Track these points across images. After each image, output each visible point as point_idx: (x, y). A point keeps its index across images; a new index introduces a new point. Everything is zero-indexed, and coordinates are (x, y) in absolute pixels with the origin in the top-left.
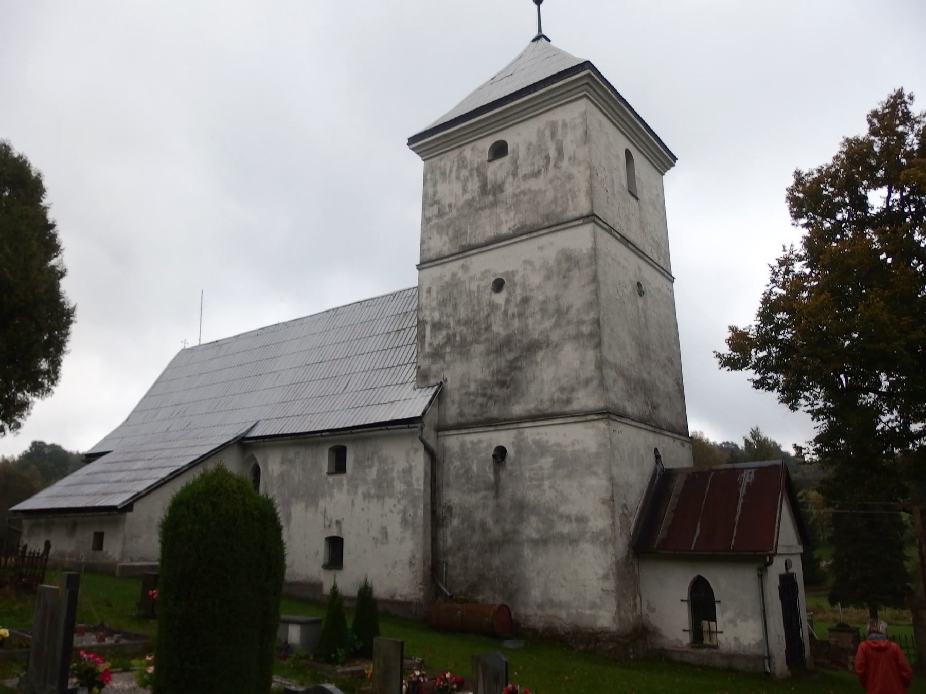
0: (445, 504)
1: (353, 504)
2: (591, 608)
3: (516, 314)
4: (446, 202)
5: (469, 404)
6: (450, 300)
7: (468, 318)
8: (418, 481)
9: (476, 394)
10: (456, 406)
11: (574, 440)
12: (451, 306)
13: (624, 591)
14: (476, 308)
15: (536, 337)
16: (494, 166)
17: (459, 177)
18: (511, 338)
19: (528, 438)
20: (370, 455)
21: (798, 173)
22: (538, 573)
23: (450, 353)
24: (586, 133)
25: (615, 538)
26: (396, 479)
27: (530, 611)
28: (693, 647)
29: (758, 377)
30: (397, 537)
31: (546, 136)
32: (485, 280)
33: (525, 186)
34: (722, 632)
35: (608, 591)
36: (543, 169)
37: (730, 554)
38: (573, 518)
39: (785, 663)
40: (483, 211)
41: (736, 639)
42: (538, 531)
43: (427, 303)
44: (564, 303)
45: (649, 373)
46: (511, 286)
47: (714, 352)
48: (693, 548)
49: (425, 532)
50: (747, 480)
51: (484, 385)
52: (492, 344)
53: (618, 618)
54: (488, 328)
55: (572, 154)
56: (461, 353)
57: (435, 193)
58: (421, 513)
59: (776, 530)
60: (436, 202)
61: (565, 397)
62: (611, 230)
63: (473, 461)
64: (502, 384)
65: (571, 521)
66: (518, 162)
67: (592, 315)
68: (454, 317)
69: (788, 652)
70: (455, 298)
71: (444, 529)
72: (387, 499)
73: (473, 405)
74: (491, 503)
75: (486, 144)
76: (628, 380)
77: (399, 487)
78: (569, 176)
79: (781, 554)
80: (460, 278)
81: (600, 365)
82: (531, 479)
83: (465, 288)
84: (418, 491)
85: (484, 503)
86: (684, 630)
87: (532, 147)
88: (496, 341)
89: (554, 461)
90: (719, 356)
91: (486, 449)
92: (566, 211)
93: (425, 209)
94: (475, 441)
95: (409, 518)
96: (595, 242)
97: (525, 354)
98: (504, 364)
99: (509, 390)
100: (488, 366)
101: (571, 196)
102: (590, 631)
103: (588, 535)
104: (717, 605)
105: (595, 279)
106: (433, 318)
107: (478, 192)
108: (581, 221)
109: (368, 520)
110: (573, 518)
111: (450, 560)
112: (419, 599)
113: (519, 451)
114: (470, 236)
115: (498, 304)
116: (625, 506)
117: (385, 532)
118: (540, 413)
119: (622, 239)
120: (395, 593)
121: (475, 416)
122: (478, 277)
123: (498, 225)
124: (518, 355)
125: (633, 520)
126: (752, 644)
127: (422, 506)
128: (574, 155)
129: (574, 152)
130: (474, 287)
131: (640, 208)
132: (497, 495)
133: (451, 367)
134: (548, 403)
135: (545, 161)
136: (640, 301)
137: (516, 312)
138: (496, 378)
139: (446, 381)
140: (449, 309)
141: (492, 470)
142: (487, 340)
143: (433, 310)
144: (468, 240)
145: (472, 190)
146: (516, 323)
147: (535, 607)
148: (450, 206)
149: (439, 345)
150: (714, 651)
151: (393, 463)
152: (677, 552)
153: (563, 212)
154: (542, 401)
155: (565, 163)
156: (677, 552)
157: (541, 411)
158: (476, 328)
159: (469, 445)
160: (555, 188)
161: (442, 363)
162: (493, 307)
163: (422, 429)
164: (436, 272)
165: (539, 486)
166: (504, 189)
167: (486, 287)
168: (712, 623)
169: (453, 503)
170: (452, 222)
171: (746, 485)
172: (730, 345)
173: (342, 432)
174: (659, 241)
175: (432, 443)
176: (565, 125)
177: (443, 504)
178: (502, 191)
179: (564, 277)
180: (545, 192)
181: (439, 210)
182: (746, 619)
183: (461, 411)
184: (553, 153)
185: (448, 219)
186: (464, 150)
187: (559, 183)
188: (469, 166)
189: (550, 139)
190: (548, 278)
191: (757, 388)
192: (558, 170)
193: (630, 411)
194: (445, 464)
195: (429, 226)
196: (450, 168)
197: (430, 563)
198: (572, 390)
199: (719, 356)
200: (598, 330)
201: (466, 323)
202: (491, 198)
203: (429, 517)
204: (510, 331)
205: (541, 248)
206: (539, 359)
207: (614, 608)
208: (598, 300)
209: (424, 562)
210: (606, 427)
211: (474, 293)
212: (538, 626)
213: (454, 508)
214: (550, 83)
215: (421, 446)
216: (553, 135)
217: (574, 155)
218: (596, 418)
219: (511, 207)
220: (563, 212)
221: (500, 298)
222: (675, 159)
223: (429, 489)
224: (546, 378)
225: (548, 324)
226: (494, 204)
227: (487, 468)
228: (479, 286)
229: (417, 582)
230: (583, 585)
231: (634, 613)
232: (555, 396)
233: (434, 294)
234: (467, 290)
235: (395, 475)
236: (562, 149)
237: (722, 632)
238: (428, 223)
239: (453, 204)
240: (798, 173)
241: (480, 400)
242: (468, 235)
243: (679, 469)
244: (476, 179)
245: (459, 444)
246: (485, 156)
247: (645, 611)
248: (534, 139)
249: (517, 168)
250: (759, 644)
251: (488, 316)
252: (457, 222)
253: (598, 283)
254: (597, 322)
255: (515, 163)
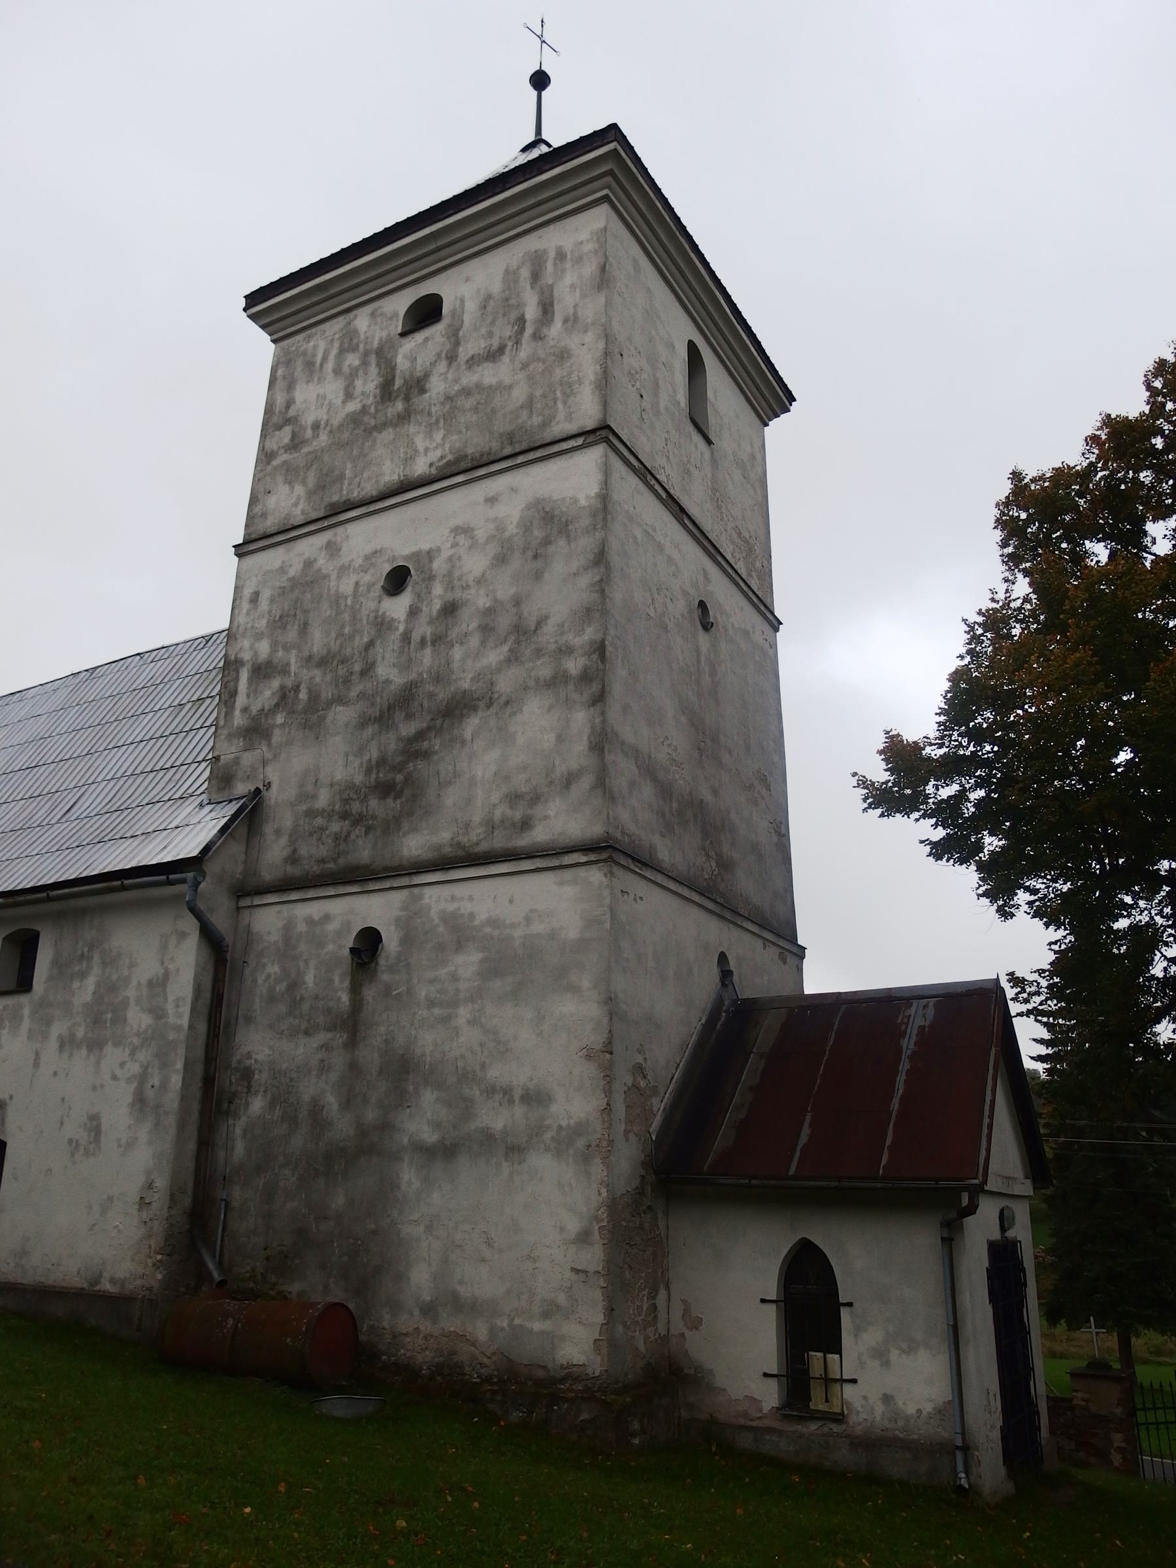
0: (239, 1062)
1: (36, 1064)
2: (546, 1315)
3: (428, 638)
4: (309, 419)
5: (311, 834)
6: (295, 615)
7: (329, 651)
8: (177, 1006)
9: (328, 814)
10: (284, 840)
11: (532, 911)
12: (296, 627)
13: (628, 1275)
14: (346, 630)
15: (465, 685)
16: (413, 344)
17: (340, 370)
18: (414, 691)
19: (430, 909)
20: (86, 950)
21: (1016, 476)
22: (429, 1228)
23: (283, 725)
24: (603, 269)
25: (611, 1142)
26: (132, 1002)
27: (405, 1322)
28: (786, 1417)
29: (940, 833)
30: (120, 1140)
31: (522, 279)
32: (372, 571)
33: (469, 379)
34: (854, 1381)
35: (586, 1272)
36: (510, 344)
37: (879, 1185)
38: (517, 1093)
39: (1001, 1460)
40: (380, 432)
41: (887, 1399)
42: (437, 1125)
43: (248, 623)
44: (531, 612)
45: (715, 792)
46: (424, 580)
47: (855, 774)
48: (792, 1172)
49: (182, 1126)
50: (920, 1021)
51: (348, 793)
52: (373, 705)
53: (609, 1342)
54: (368, 670)
55: (571, 311)
56: (305, 726)
57: (289, 404)
58: (176, 1080)
59: (985, 1131)
60: (288, 421)
61: (517, 815)
62: (645, 473)
63: (306, 962)
64: (386, 790)
65: (511, 1102)
66: (461, 333)
67: (590, 633)
68: (300, 651)
69: (1007, 1433)
70: (306, 612)
71: (231, 1122)
72: (109, 1049)
73: (319, 839)
74: (339, 1060)
75: (401, 303)
76: (665, 790)
77: (138, 1019)
78: (562, 352)
79: (992, 1193)
80: (320, 570)
81: (601, 741)
82: (431, 1004)
83: (329, 589)
84: (178, 1028)
85: (322, 1061)
86: (766, 1375)
87: (492, 303)
88: (382, 697)
89: (481, 962)
90: (863, 783)
91: (339, 934)
92: (551, 421)
93: (265, 435)
94: (316, 918)
95: (150, 1094)
96: (606, 483)
97: (439, 722)
98: (392, 747)
99: (398, 801)
100: (360, 751)
101: (564, 393)
102: (540, 1374)
103: (548, 1136)
104: (845, 1313)
105: (600, 558)
106: (256, 654)
107: (375, 397)
108: (580, 441)
109: (63, 1099)
110: (517, 1093)
111: (237, 1194)
112: (150, 1289)
113: (407, 940)
114: (350, 484)
115: (393, 620)
116: (639, 1069)
117: (95, 1127)
118: (460, 853)
119: (670, 502)
120: (101, 1275)
121: (322, 861)
122: (357, 566)
123: (409, 459)
124: (425, 725)
125: (659, 1105)
126: (925, 1413)
127: (179, 1065)
128: (575, 314)
129: (576, 306)
130: (347, 586)
131: (714, 462)
132: (352, 1043)
133: (283, 756)
134: (480, 830)
135: (516, 327)
136: (703, 639)
137: (428, 634)
138: (373, 776)
139: (268, 786)
140: (292, 635)
141: (347, 983)
142: (362, 696)
143: (258, 637)
144: (345, 492)
145: (363, 393)
146: (427, 657)
147: (417, 1313)
148: (316, 426)
149: (263, 710)
150: (835, 1428)
151: (132, 965)
152: (754, 1182)
153: (545, 425)
154: (467, 826)
155: (555, 330)
156: (754, 1182)
157: (463, 848)
158: (342, 671)
159: (301, 927)
160: (530, 378)
161: (265, 748)
162: (382, 624)
163: (196, 884)
164: (271, 559)
165: (446, 1020)
166: (427, 386)
167: (370, 586)
168: (833, 1358)
169: (256, 1061)
170: (316, 457)
171: (915, 1032)
172: (887, 760)
173: (29, 897)
174: (752, 542)
175: (220, 921)
176: (561, 256)
177: (234, 1065)
178: (423, 391)
179: (535, 557)
180: (510, 387)
181: (294, 436)
182: (911, 1349)
183: (295, 851)
184: (531, 312)
185: (310, 453)
186: (356, 317)
187: (540, 367)
188: (361, 346)
189: (529, 288)
190: (501, 560)
191: (938, 857)
192: (540, 343)
193: (667, 859)
194: (247, 972)
195: (269, 468)
196: (324, 353)
197: (187, 1201)
198: (536, 799)
199: (863, 783)
200: (601, 667)
201: (323, 662)
202: (400, 406)
203: (196, 1091)
204: (413, 676)
205: (491, 500)
206: (468, 734)
207: (600, 1318)
208: (603, 603)
209: (172, 1196)
210: (605, 880)
211: (346, 598)
212: (420, 1358)
213: (256, 1072)
214: (535, 173)
215: (190, 925)
216: (536, 276)
217: (575, 314)
218: (584, 859)
219: (437, 421)
220: (545, 425)
221: (397, 607)
222: (792, 399)
223: (202, 1027)
224: (480, 774)
225: (494, 657)
226: (404, 418)
227: (337, 979)
228: (357, 584)
229: (150, 1246)
230: (529, 1257)
231: (652, 1329)
232: (498, 814)
233: (264, 604)
234: (332, 592)
235: (131, 993)
236: (552, 304)
237: (854, 1381)
238: (268, 463)
239: (322, 423)
240: (1016, 476)
241: (336, 827)
242: (346, 482)
243: (772, 1000)
244: (373, 370)
245: (280, 924)
246: (397, 326)
247: (678, 1325)
248: (496, 287)
249: (457, 344)
250: (940, 1411)
251: (370, 645)
252: (326, 458)
253: (608, 567)
254: (600, 649)
255: (455, 338)
